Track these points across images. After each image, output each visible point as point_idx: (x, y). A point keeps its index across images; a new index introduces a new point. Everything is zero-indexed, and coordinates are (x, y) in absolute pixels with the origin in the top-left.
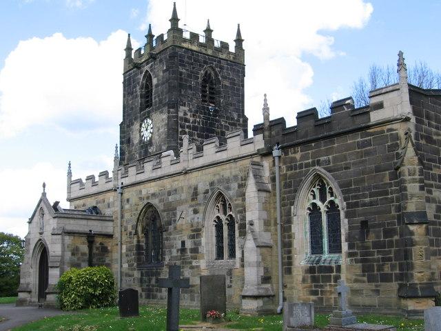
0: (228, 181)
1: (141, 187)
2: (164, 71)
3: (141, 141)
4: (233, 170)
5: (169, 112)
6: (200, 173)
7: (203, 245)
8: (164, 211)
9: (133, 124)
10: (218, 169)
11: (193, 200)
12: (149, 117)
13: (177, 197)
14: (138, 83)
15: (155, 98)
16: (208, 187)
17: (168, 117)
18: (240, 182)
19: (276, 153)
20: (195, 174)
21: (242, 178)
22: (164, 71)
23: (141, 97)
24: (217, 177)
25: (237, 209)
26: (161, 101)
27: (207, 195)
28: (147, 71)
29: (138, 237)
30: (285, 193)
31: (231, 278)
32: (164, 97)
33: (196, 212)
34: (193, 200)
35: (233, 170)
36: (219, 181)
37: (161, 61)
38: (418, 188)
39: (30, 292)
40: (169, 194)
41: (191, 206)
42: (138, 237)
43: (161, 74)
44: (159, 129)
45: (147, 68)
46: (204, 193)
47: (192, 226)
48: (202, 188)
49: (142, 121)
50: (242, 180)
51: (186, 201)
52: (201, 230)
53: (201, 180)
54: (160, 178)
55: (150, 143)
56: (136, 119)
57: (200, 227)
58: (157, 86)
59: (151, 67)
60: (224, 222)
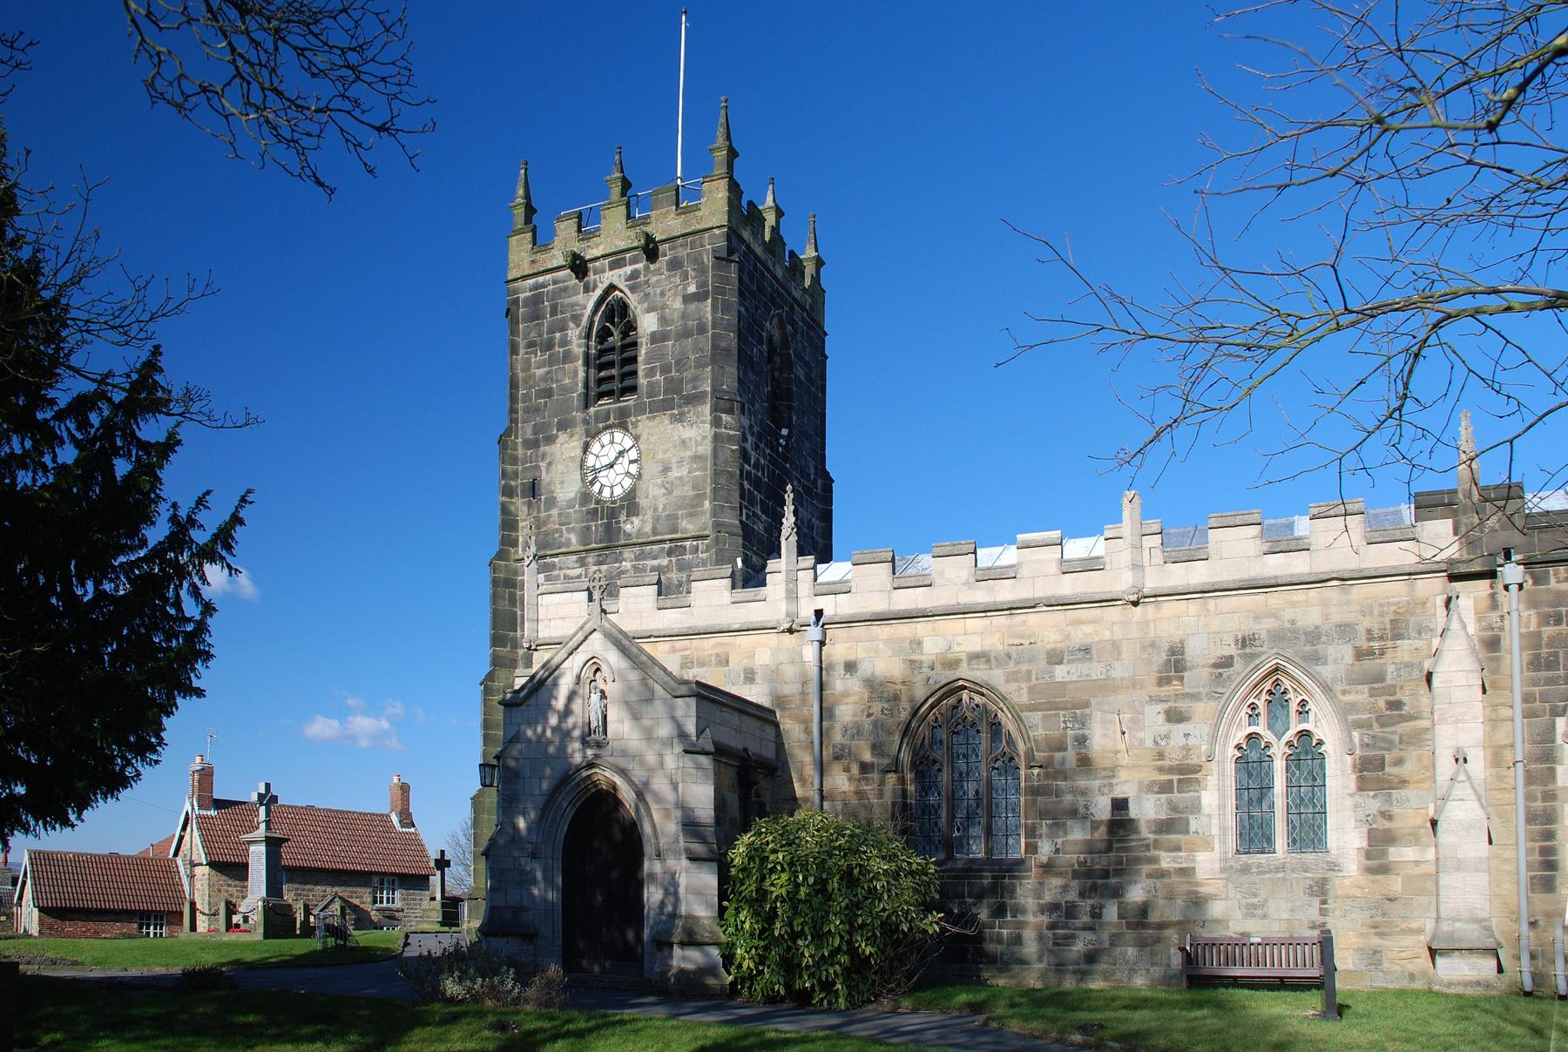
0: (1314, 636)
1: (920, 628)
2: (687, 299)
3: (585, 497)
4: (1333, 609)
5: (716, 422)
6: (1060, 615)
7: (1206, 809)
8: (1032, 708)
9: (551, 440)
10: (1275, 599)
11: (1163, 681)
12: (623, 426)
13: (1096, 670)
14: (576, 319)
15: (650, 373)
16: (1232, 650)
17: (717, 438)
18: (1365, 645)
19: (1512, 572)
20: (1171, 607)
21: (1369, 631)
22: (687, 299)
23: (587, 363)
24: (1269, 624)
25: (1350, 718)
26: (674, 387)
27: (1226, 672)
28: (612, 288)
29: (902, 781)
30: (1534, 683)
31: (1324, 902)
32: (687, 375)
33: (1175, 717)
34: (1163, 681)
35: (1333, 609)
36: (1278, 637)
37: (675, 265)
38: (1161, 717)
39: (529, 937)
40: (1055, 658)
41: (1153, 700)
42: (902, 781)
43: (678, 304)
44: (666, 470)
45: (617, 277)
46: (1215, 666)
47: (1161, 756)
48: (1200, 652)
49: (593, 435)
50: (1369, 640)
51: (1135, 684)
52: (1197, 769)
53: (1205, 630)
54: (1011, 608)
55: (630, 503)
56: (563, 426)
57: (1193, 760)
58: (655, 338)
59: (634, 275)
60: (1279, 751)
